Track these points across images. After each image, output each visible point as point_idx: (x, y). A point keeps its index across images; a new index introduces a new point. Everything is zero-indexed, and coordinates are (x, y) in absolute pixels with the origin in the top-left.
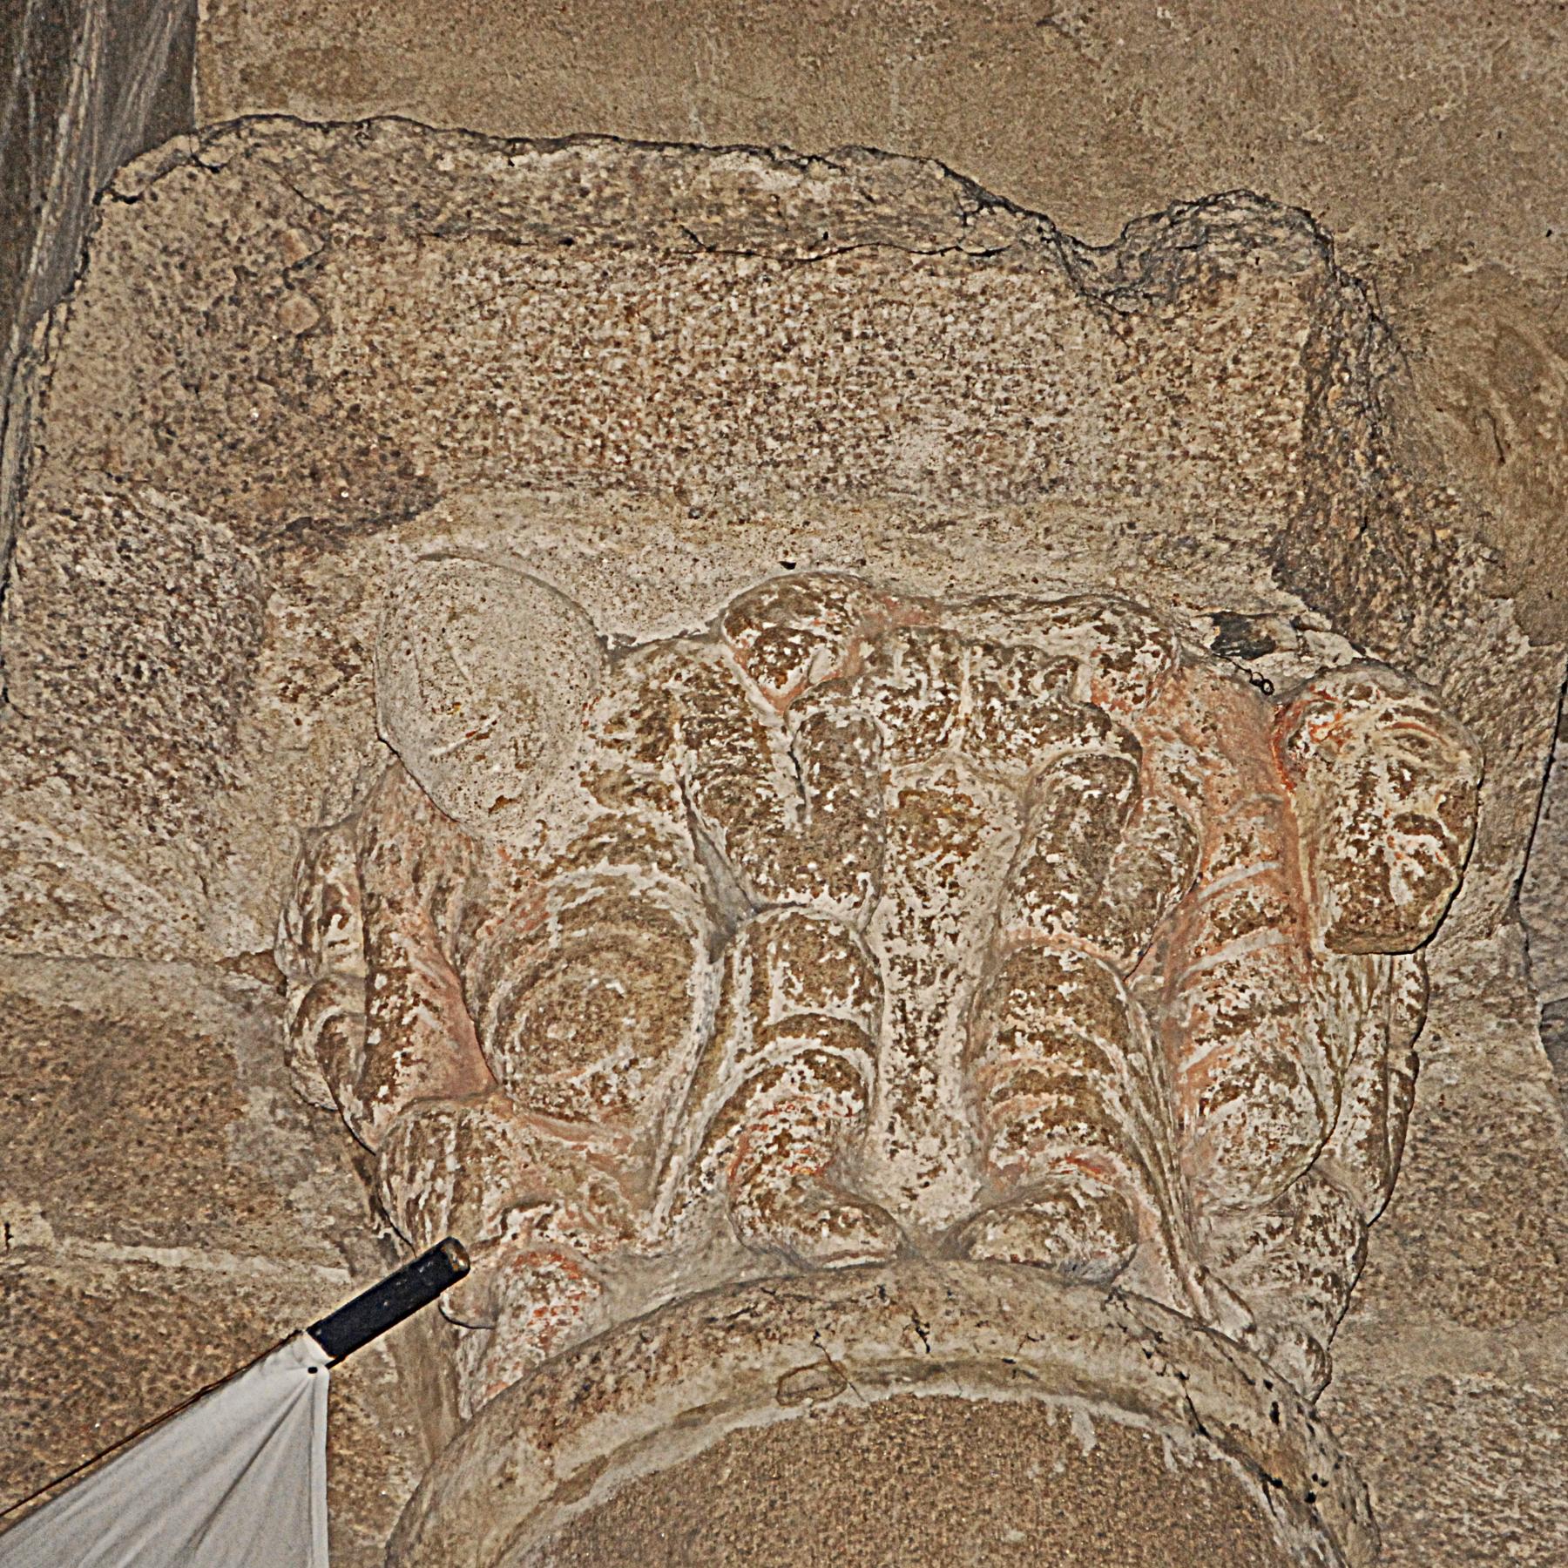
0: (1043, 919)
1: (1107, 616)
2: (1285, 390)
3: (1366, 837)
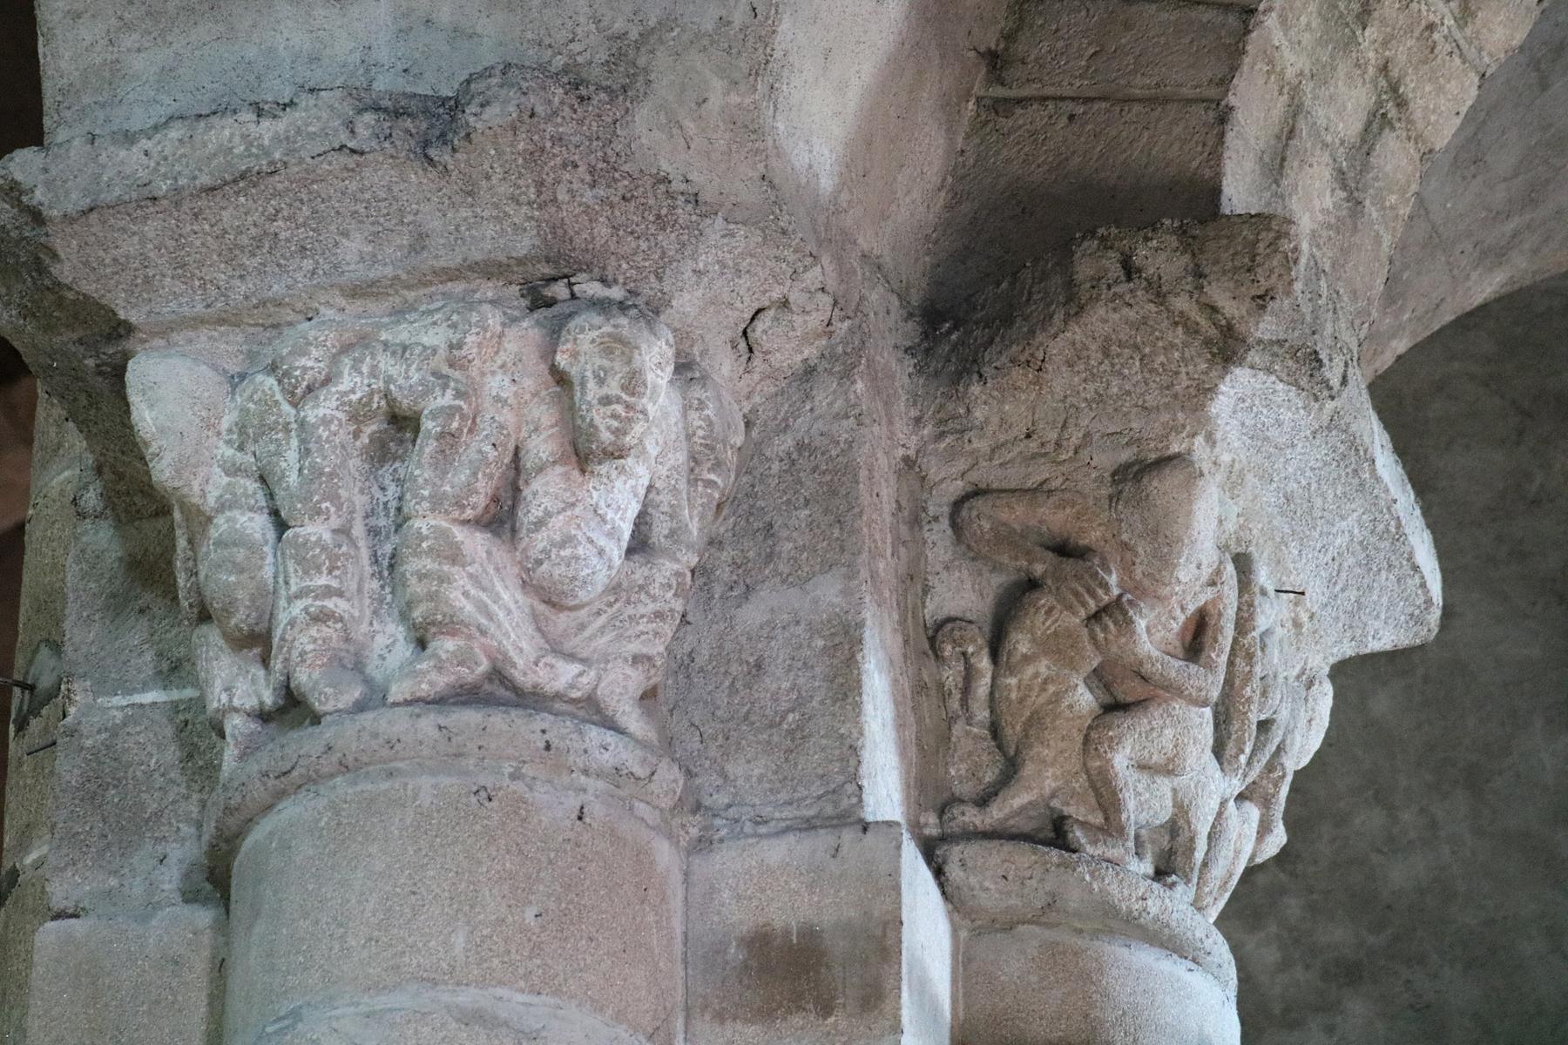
2: (520, 176)
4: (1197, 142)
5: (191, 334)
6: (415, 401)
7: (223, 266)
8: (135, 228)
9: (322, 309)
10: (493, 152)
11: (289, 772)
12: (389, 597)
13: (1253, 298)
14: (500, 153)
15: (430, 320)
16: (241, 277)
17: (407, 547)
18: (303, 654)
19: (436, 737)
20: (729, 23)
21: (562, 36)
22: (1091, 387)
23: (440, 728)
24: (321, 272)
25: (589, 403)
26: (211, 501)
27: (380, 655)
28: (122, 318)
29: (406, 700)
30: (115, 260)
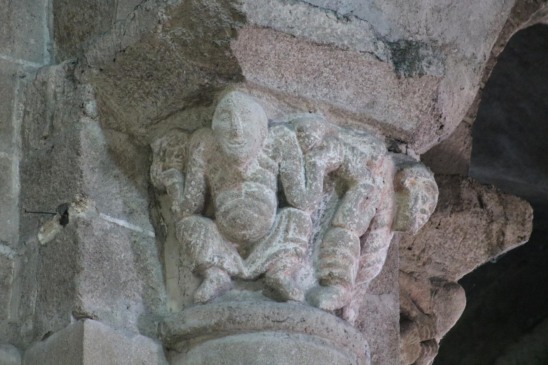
0: (349, 225)
1: (374, 144)
3: (414, 212)
4: (462, 140)
5: (260, 94)
6: (357, 177)
7: (294, 74)
8: (274, 42)
9: (318, 111)
10: (424, 85)
11: (281, 322)
12: (311, 253)
13: (519, 237)
14: (426, 86)
15: (361, 139)
16: (298, 82)
17: (343, 241)
18: (285, 266)
19: (344, 335)
20: (476, 58)
21: (414, 29)
22: (440, 240)
23: (345, 331)
24: (328, 96)
25: (417, 209)
26: (249, 173)
27: (301, 278)
28: (243, 75)
29: (327, 310)
30: (257, 50)
